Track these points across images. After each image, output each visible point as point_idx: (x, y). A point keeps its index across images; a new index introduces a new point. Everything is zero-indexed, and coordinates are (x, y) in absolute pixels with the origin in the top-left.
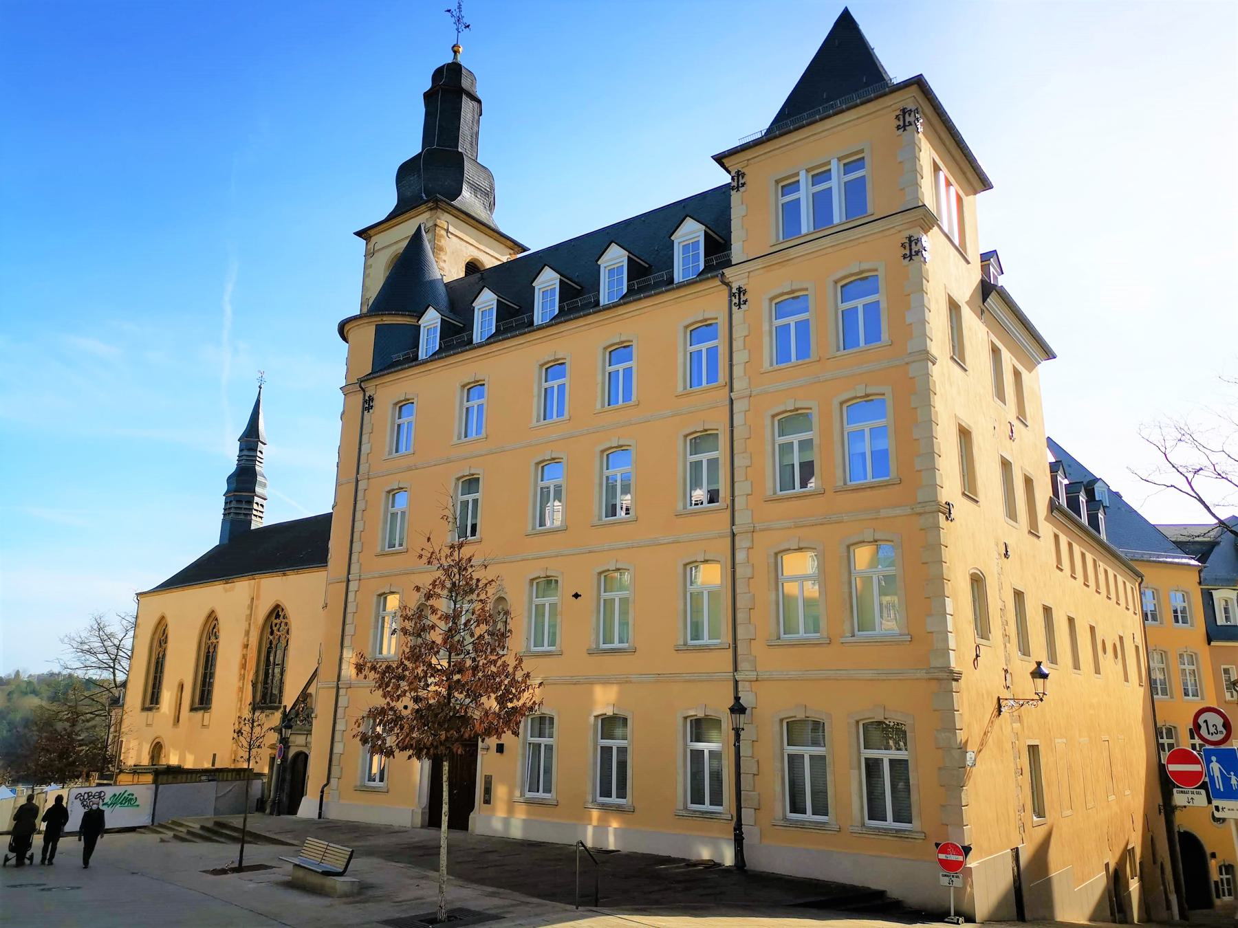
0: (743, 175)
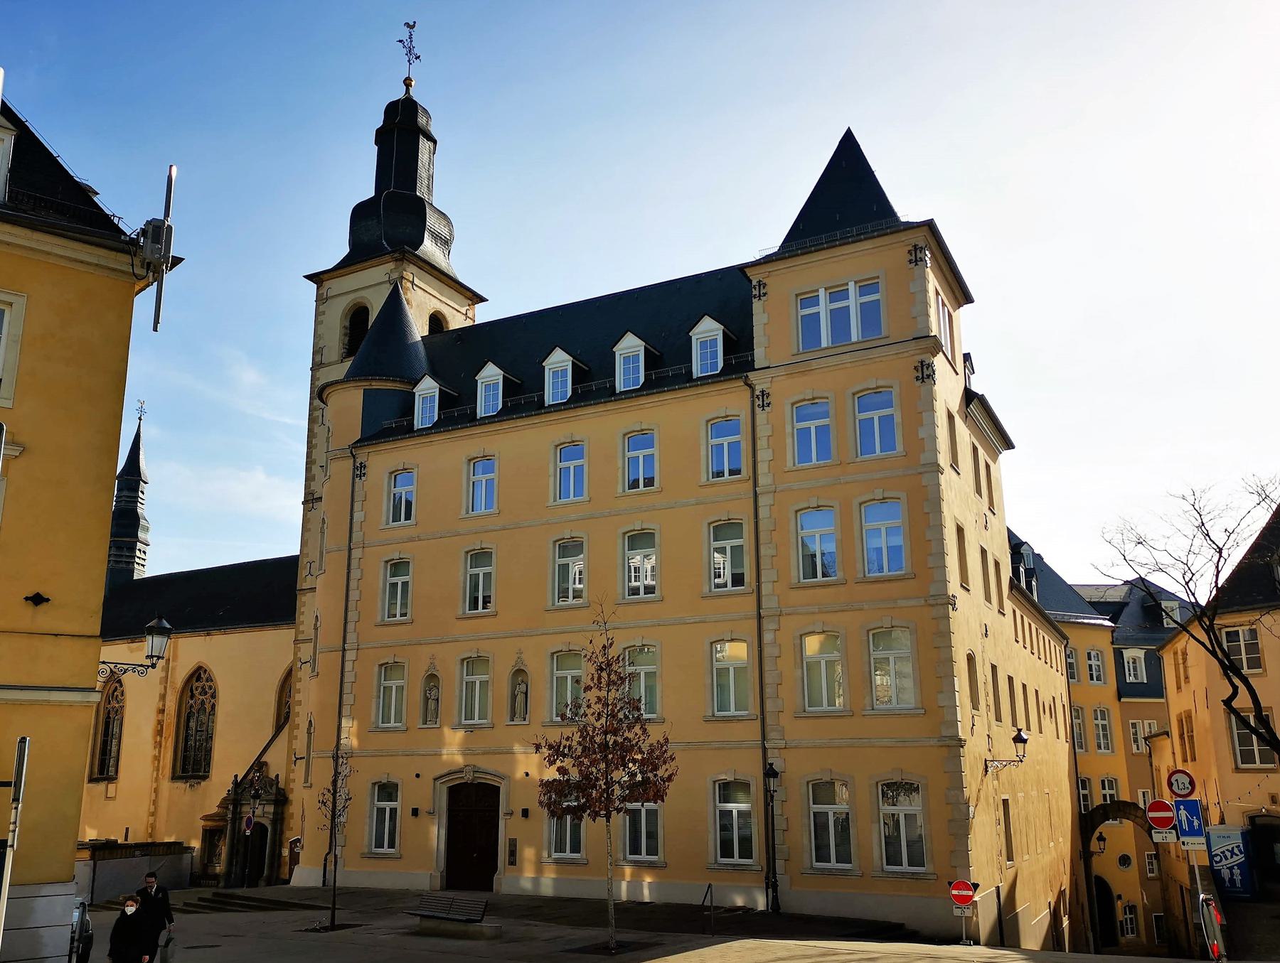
0: (765, 285)
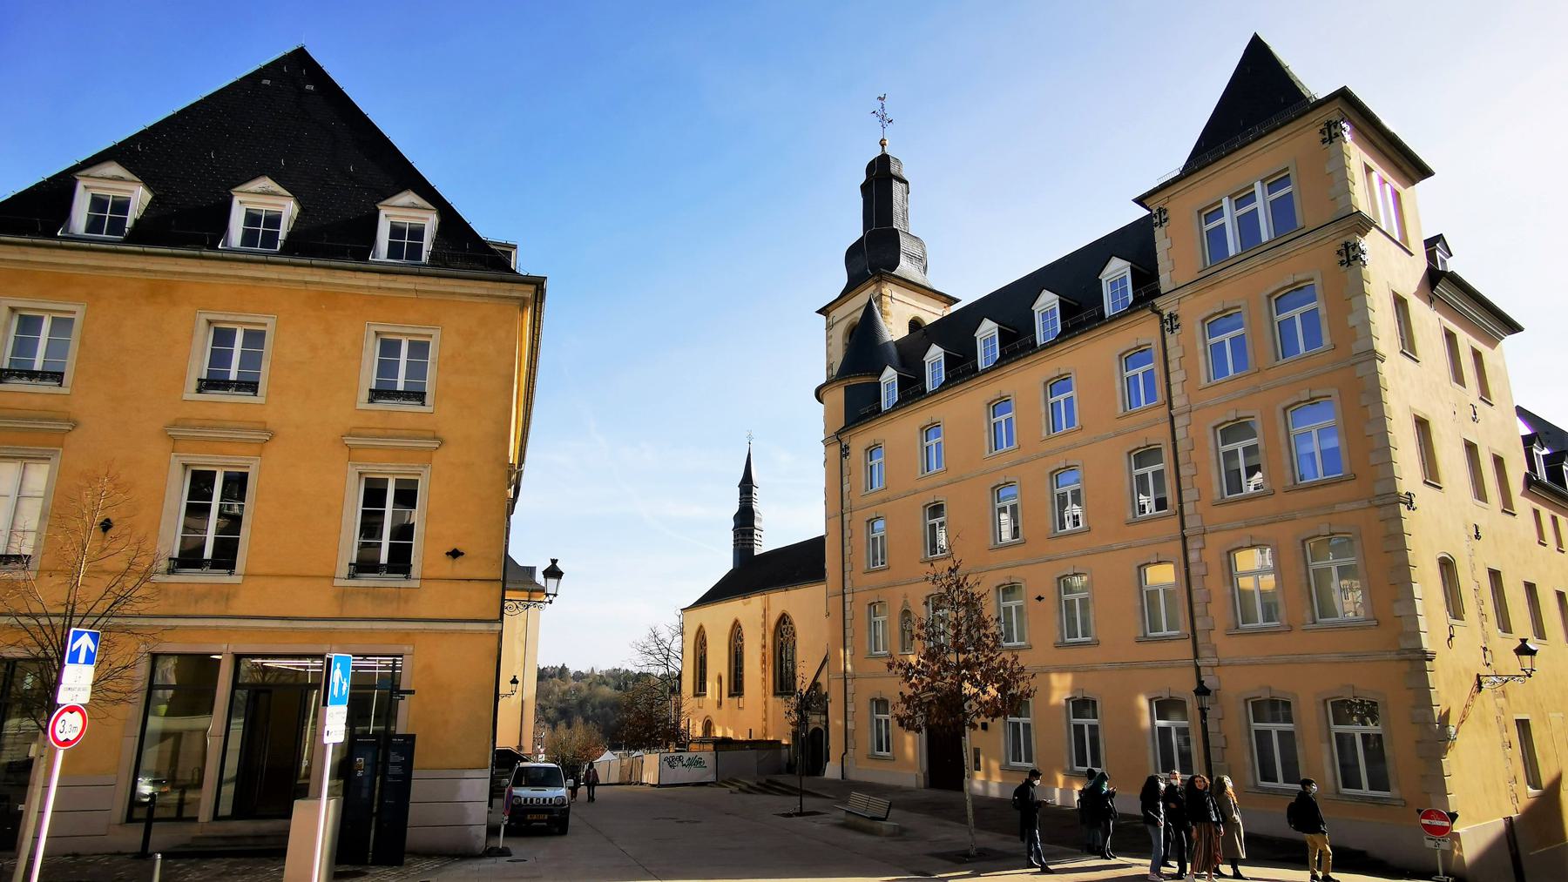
0: (1165, 211)
